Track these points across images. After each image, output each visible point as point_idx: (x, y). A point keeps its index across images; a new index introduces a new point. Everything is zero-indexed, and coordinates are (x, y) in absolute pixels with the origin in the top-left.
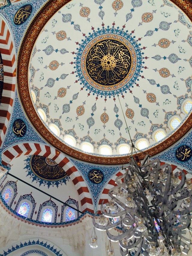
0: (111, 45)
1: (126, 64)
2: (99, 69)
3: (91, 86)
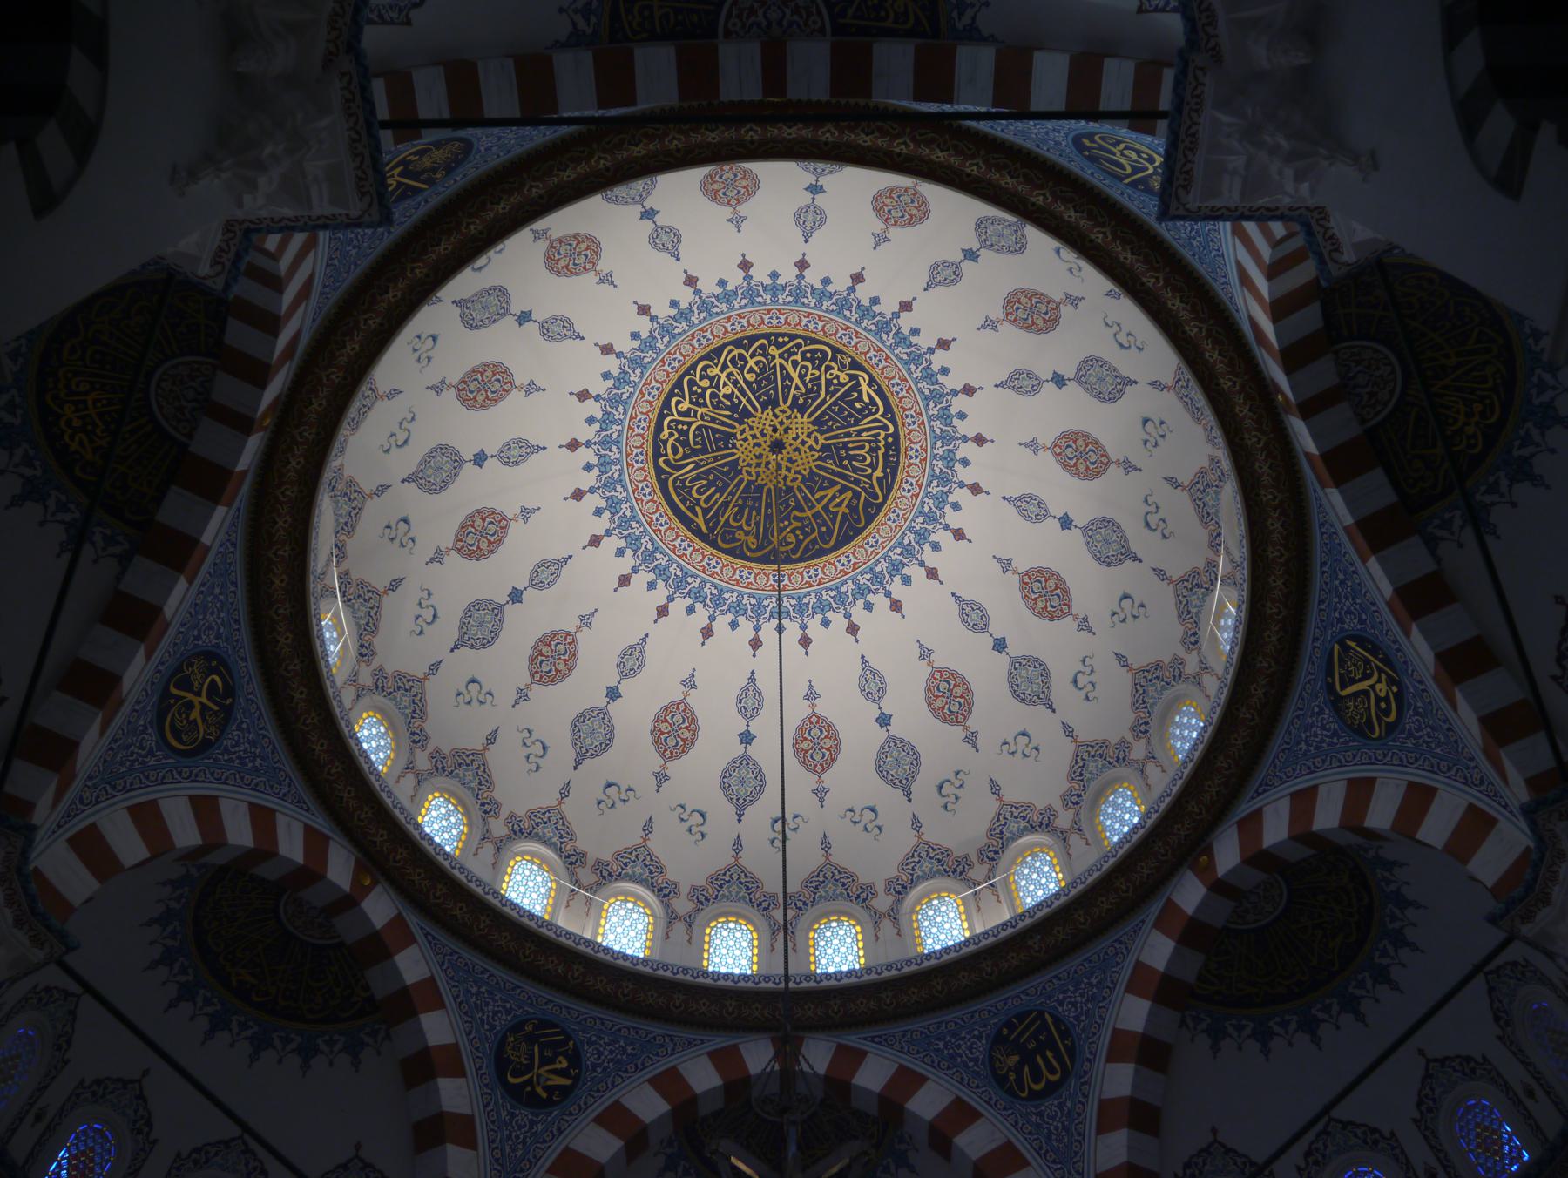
0: (869, 442)
1: (791, 538)
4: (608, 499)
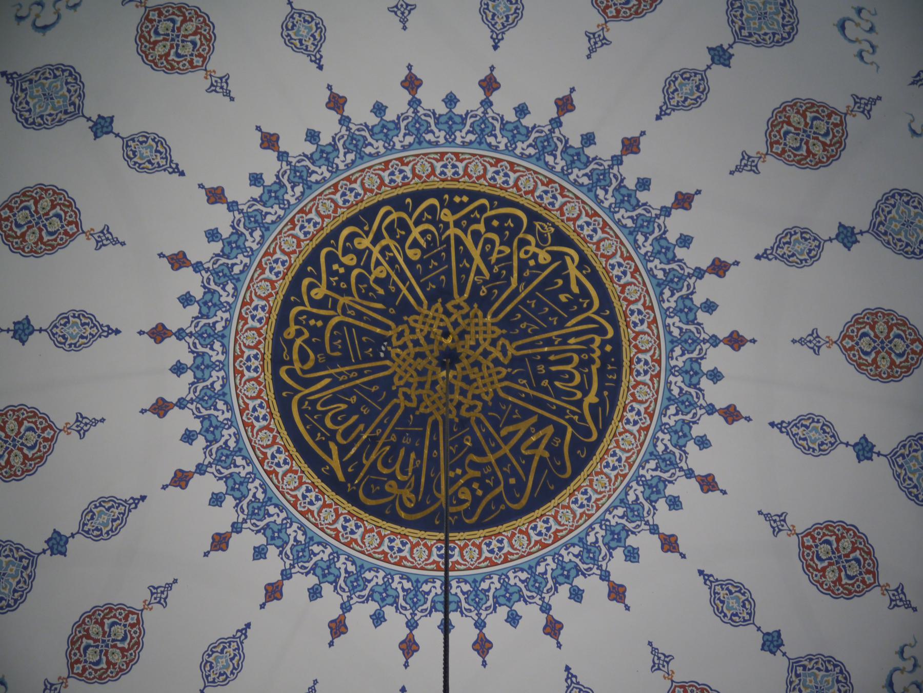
0: (579, 352)
1: (465, 495)
2: (389, 298)
3: (247, 267)
4: (203, 419)
